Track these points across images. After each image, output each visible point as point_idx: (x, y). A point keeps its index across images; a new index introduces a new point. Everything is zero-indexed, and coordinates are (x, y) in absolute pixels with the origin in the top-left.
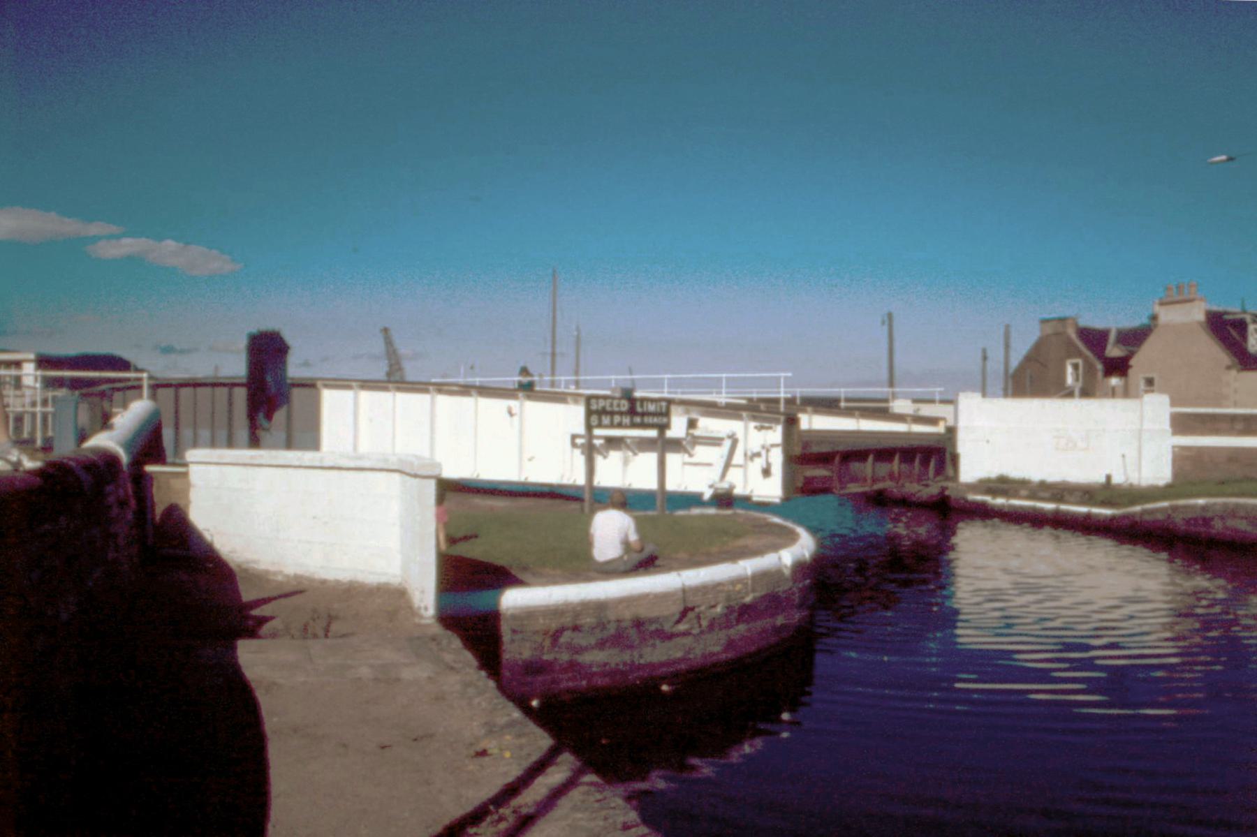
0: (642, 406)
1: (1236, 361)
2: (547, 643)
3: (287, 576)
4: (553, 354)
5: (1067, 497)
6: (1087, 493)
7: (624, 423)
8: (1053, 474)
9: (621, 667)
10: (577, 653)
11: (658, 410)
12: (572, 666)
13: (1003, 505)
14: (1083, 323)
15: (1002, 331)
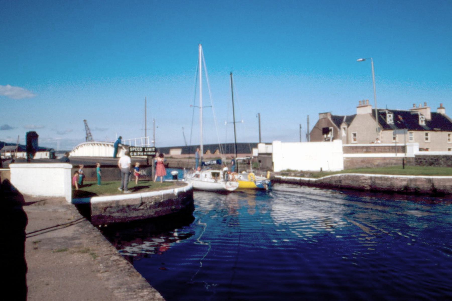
0: (147, 149)
1: (381, 127)
2: (103, 211)
3: (37, 196)
4: (146, 129)
5: (305, 175)
6: (312, 174)
7: (141, 154)
8: (305, 168)
9: (124, 218)
10: (111, 213)
11: (152, 150)
12: (110, 216)
13: (285, 179)
14: (334, 114)
15: (306, 118)
